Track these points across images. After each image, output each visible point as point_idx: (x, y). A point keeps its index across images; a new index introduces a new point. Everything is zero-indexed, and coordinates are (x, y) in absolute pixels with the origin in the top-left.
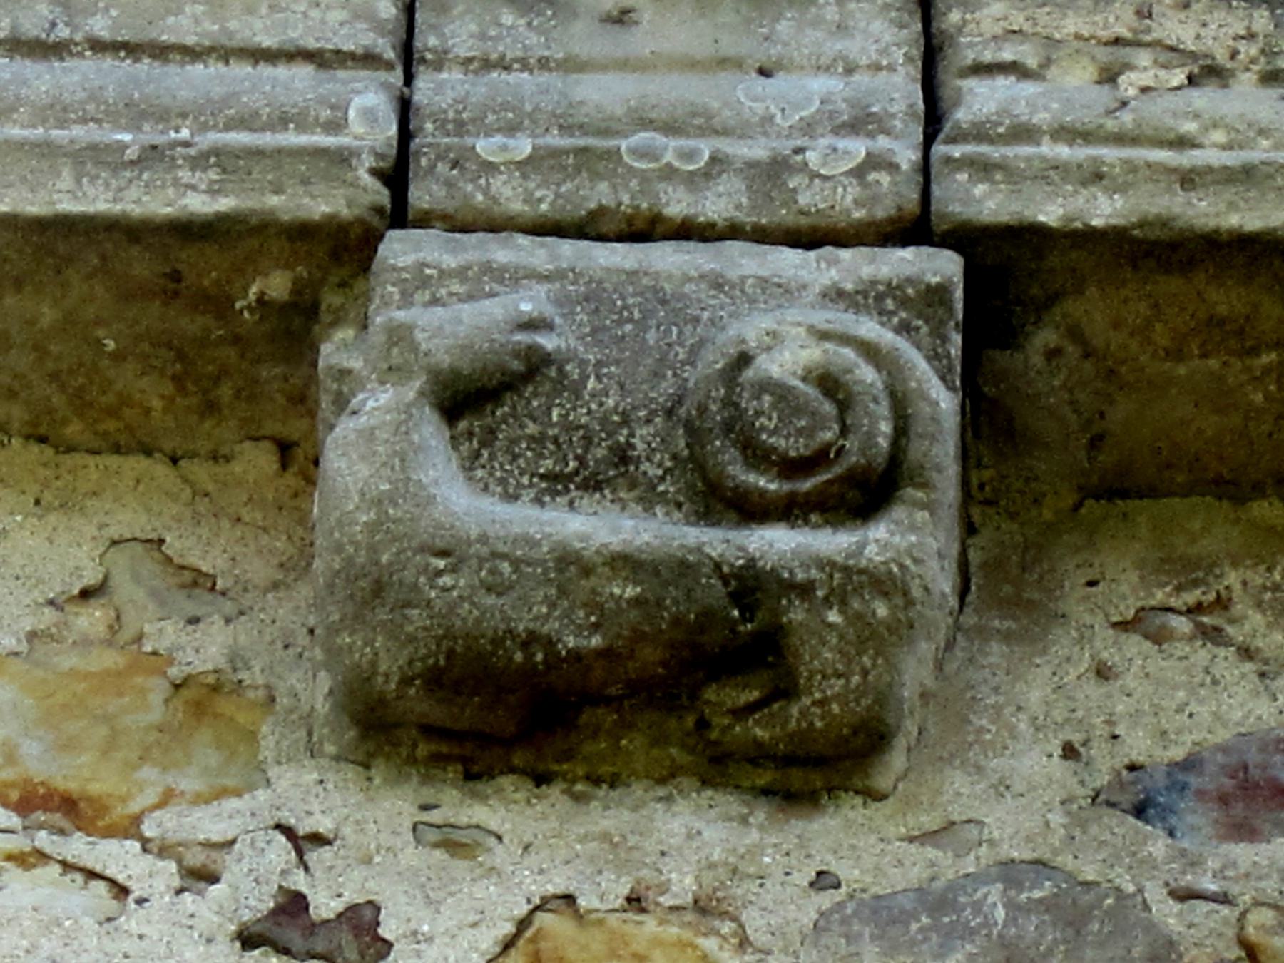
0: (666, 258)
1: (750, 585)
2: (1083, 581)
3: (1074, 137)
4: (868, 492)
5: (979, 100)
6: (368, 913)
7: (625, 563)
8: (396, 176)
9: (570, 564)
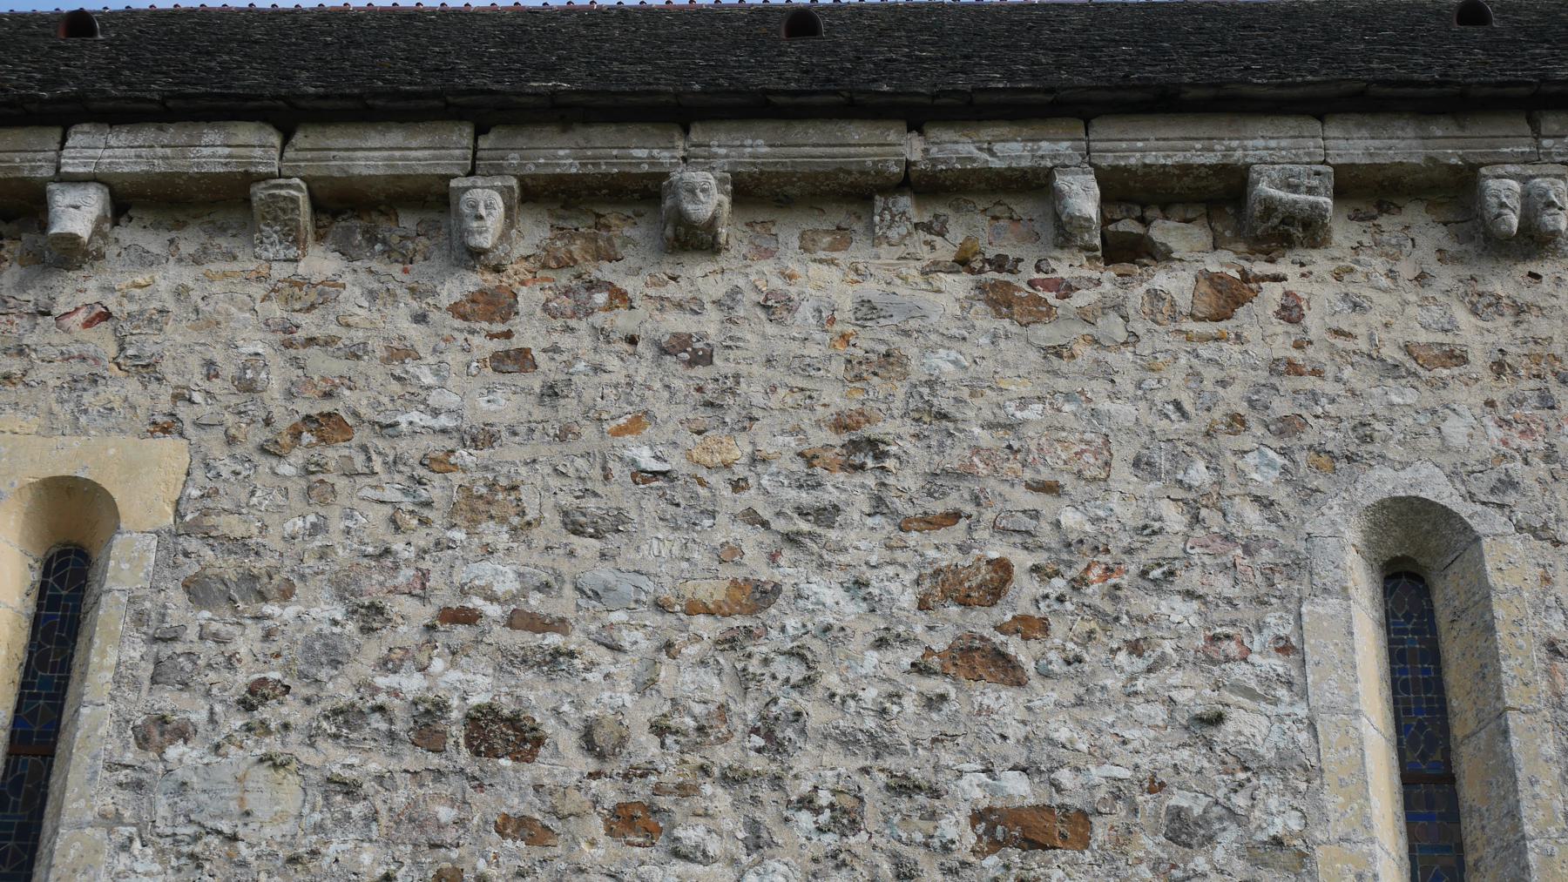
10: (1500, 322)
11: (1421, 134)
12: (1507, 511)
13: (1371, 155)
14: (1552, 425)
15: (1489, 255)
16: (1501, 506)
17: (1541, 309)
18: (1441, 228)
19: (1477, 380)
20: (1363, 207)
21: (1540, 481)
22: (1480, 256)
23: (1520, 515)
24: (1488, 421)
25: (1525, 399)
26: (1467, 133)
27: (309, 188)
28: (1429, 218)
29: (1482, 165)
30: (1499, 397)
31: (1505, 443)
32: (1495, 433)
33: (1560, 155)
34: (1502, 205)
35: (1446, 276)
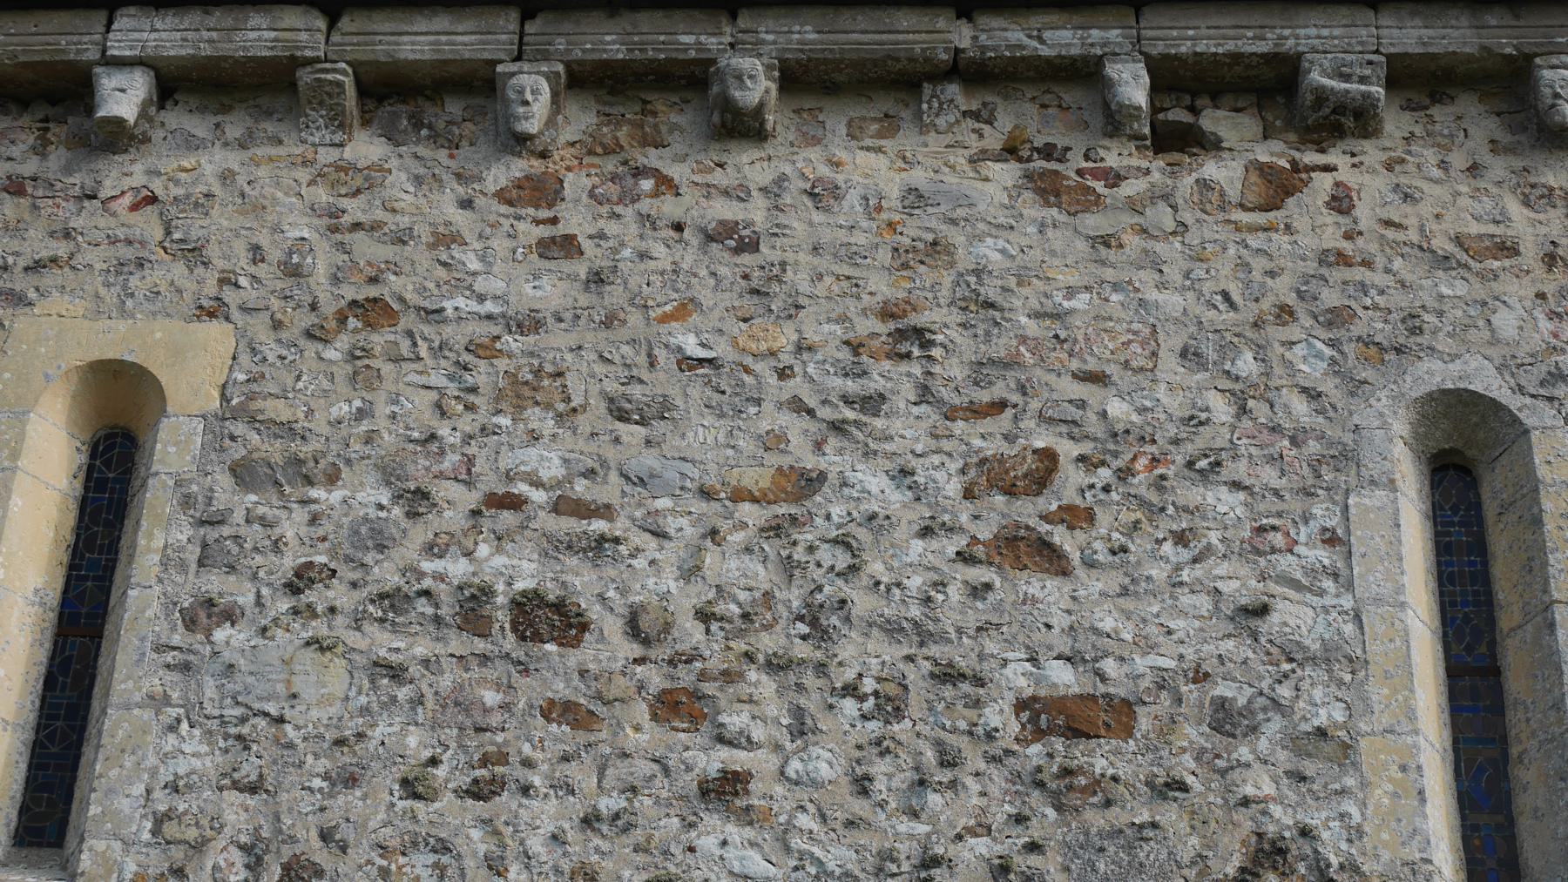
12: (1556, 404)
13: (1424, 44)
16: (1551, 399)
19: (1528, 272)
22: (1533, 147)
24: (1539, 314)
26: (1522, 23)
28: (1482, 108)
34: (1557, 96)
35: (1498, 168)
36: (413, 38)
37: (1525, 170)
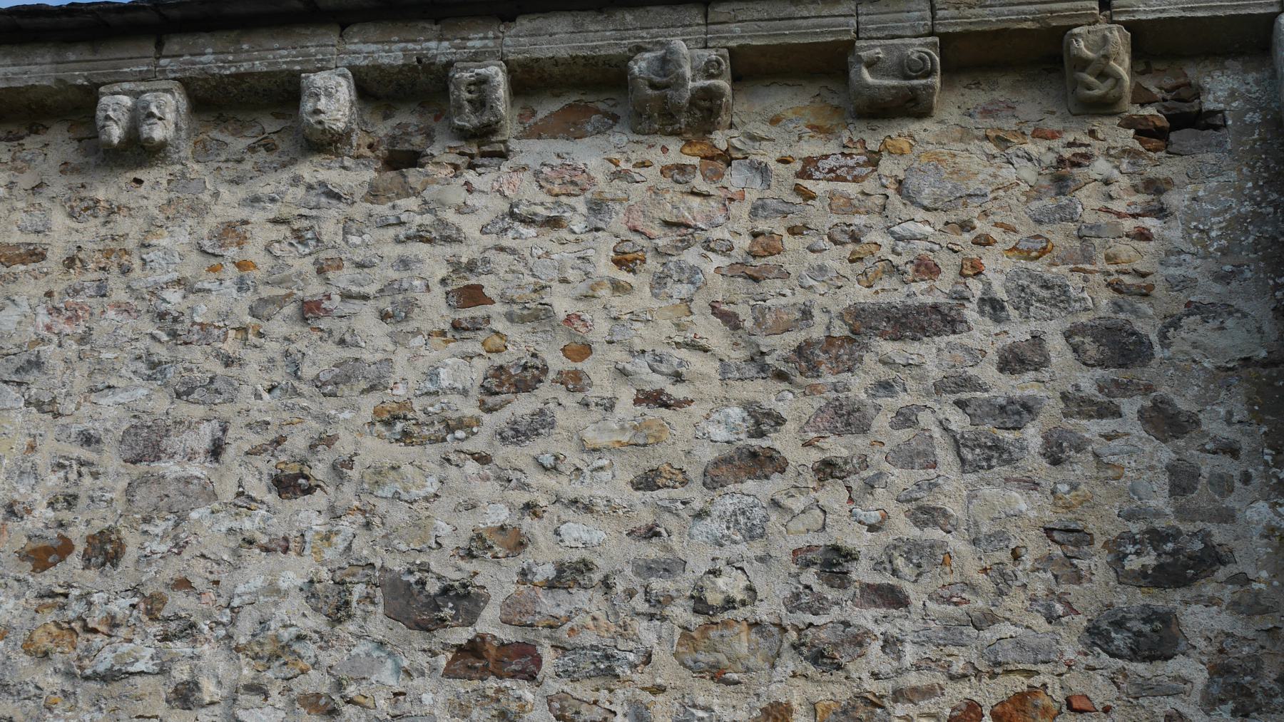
0: (896, 41)
1: (912, 89)
2: (778, 155)
3: (954, 19)
4: (929, 74)
5: (940, 14)
6: (1142, 67)
7: (894, 87)
8: (857, 32)
9: (887, 88)
10: (93, 222)
11: (57, 59)
12: (23, 388)
13: (7, 79)
14: (97, 311)
15: (107, 165)
16: (20, 384)
17: (130, 209)
18: (76, 144)
19: (47, 274)
20: (14, 129)
21: (66, 361)
22: (97, 166)
23: (33, 391)
24: (42, 311)
25: (83, 289)
26: (98, 57)
27: (354, 75)
28: (67, 135)
29: (104, 84)
30: (57, 288)
31: (49, 328)
32: (43, 318)
33: (174, 71)
34: (108, 118)
35: (58, 185)
36: (719, 27)
37: (83, 186)
